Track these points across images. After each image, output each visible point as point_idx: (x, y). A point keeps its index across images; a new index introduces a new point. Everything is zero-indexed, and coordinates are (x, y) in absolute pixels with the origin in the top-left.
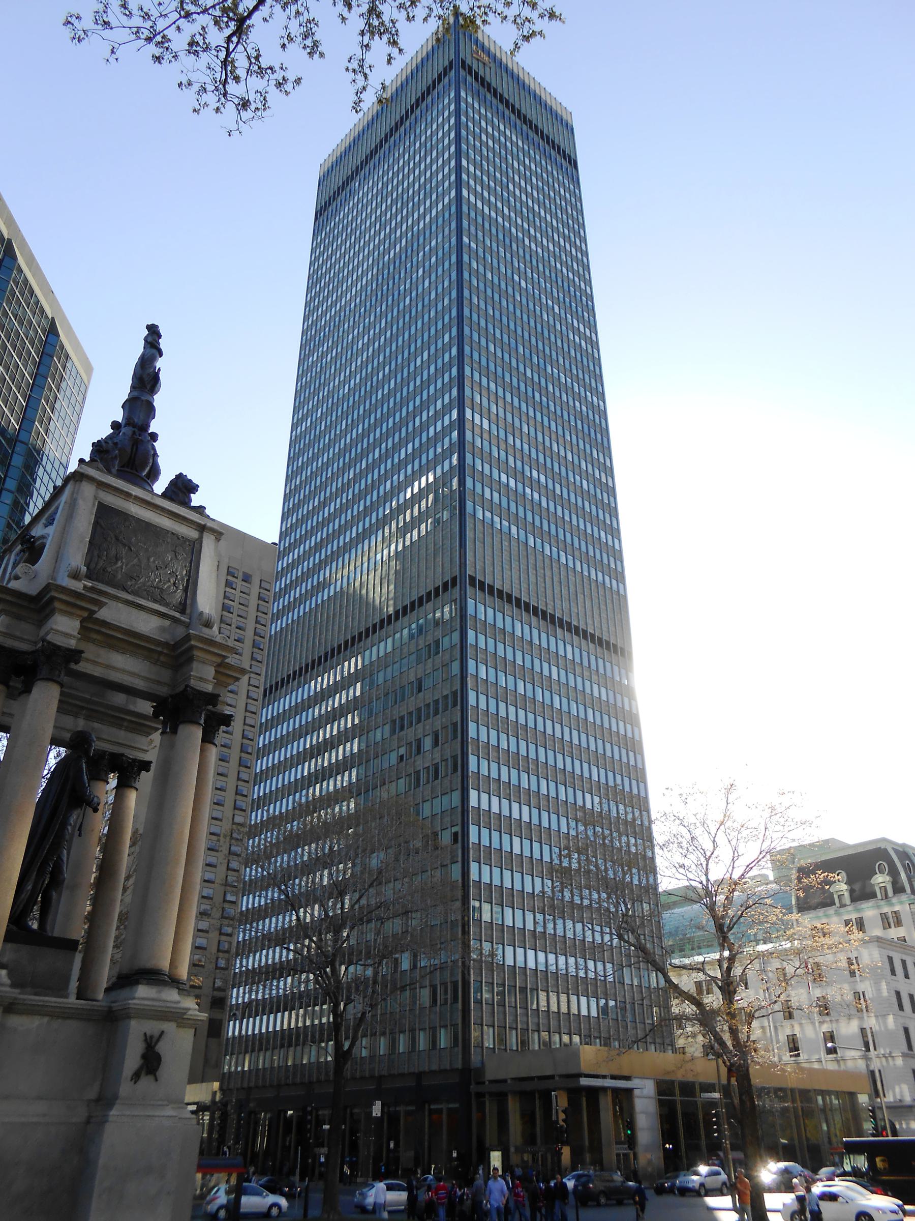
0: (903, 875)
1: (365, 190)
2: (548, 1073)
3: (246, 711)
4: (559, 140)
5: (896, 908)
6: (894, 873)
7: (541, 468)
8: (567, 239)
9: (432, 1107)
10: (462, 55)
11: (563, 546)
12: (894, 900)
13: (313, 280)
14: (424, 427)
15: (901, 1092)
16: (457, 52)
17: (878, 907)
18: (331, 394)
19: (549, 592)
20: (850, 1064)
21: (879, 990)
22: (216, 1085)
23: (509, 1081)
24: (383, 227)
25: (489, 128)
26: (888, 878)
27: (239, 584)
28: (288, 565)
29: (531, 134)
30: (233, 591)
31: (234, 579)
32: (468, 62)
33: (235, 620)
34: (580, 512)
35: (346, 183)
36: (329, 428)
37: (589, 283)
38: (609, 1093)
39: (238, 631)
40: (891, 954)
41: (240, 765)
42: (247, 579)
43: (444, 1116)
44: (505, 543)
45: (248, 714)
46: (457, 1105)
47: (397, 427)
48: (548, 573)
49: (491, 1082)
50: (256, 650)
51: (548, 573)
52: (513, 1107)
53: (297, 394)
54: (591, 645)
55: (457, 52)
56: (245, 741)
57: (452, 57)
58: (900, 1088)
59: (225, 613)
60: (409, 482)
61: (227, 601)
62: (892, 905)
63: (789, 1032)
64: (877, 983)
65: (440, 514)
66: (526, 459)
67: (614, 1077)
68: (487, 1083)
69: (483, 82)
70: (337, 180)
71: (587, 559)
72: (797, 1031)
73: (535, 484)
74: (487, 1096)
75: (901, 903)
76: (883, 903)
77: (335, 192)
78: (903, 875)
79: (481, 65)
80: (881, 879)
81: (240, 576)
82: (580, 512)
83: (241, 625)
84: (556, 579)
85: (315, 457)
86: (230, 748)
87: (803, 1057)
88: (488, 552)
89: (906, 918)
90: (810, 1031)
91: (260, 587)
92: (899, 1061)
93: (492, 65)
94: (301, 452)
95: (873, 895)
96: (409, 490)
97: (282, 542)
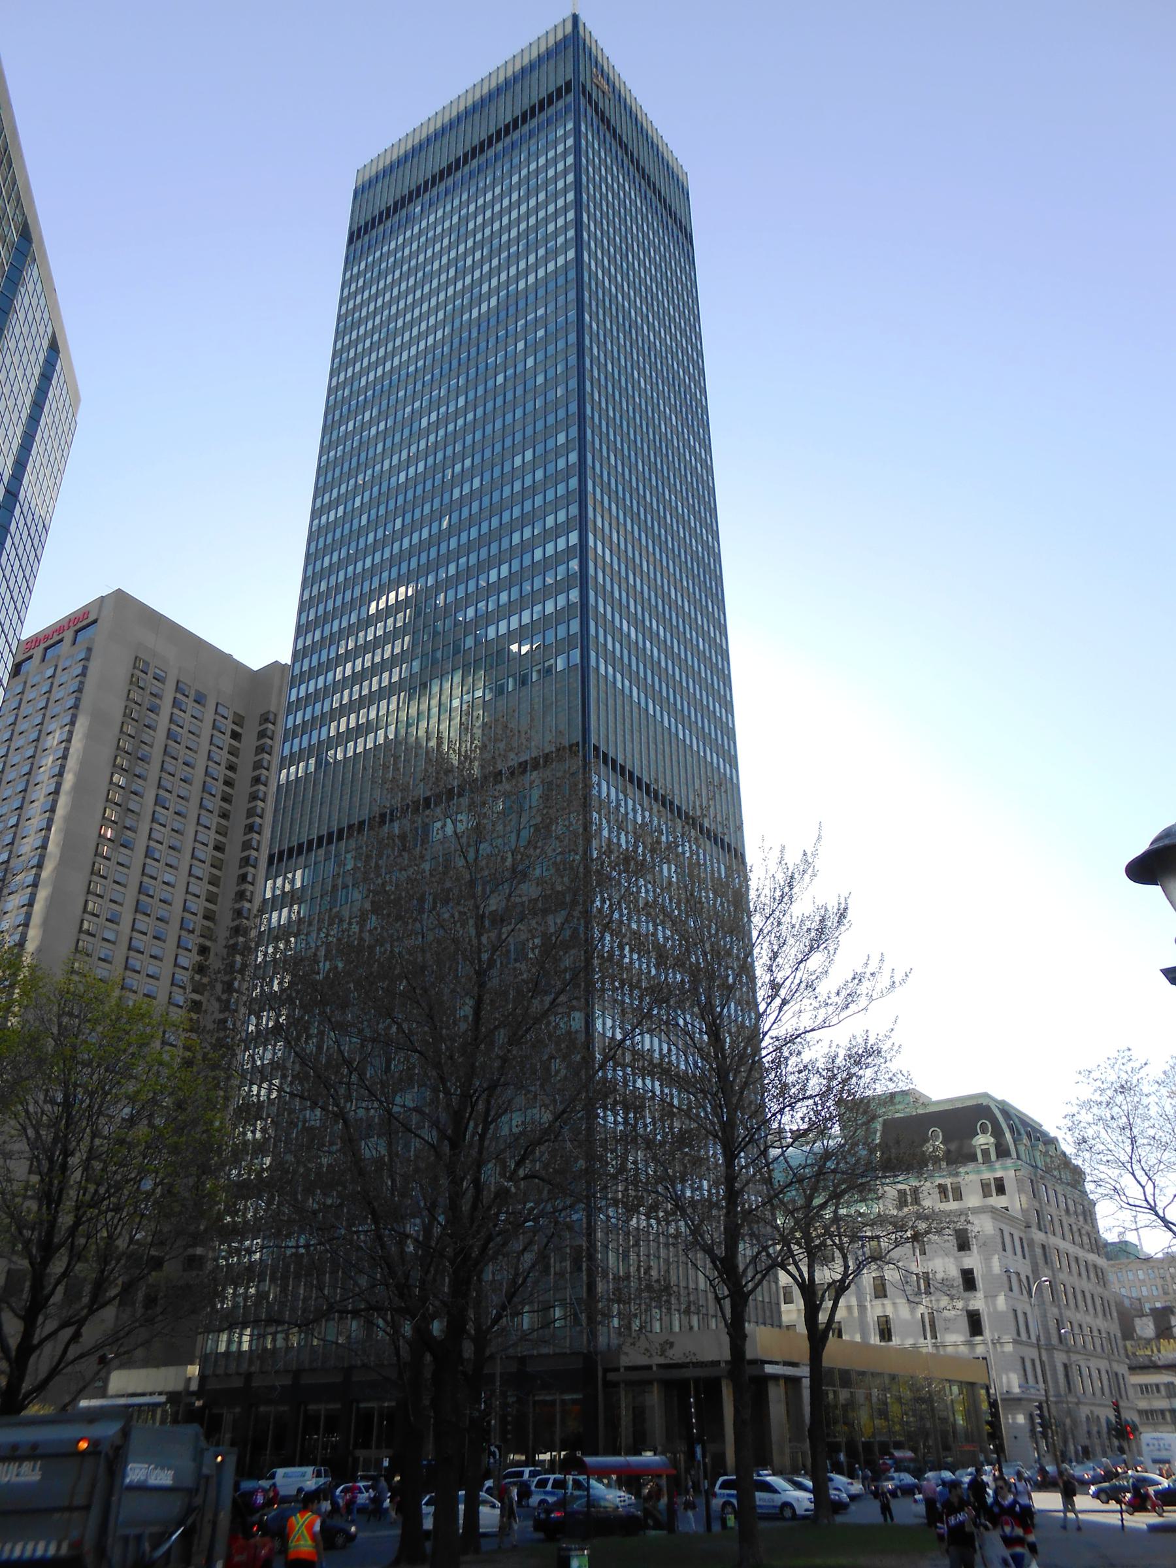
0: (1008, 1135)
1: (434, 220)
2: (716, 1358)
3: (190, 875)
4: (676, 205)
5: (998, 1175)
6: (998, 1133)
7: (660, 618)
8: (683, 332)
9: (537, 1398)
10: (582, 79)
11: (684, 720)
12: (998, 1165)
13: (346, 324)
14: (527, 547)
15: (1009, 1382)
16: (576, 71)
17: (979, 1172)
18: (377, 480)
19: (668, 772)
20: (950, 1350)
21: (989, 1267)
22: (194, 1370)
23: (655, 1368)
24: (461, 274)
25: (609, 180)
26: (992, 1140)
27: (190, 705)
28: (308, 695)
29: (650, 193)
30: (182, 714)
31: (184, 698)
32: (588, 88)
33: (182, 753)
34: (694, 675)
35: (400, 204)
36: (374, 524)
37: (704, 391)
38: (782, 1382)
39: (186, 768)
40: (1004, 1227)
41: (178, 947)
42: (199, 700)
43: (558, 1408)
44: (627, 708)
45: (192, 880)
46: (338, 1406)
47: (484, 540)
48: (667, 749)
49: (628, 1368)
50: (206, 795)
51: (667, 749)
52: (654, 1398)
53: (321, 471)
54: (708, 842)
55: (576, 71)
56: (187, 915)
57: (570, 76)
58: (1008, 1378)
59: (171, 742)
60: (383, 590)
61: (173, 727)
62: (994, 1170)
63: (879, 1312)
64: (987, 1260)
65: (552, 661)
66: (646, 605)
67: (786, 1364)
68: (622, 1370)
69: (603, 118)
70: (385, 197)
71: (703, 737)
72: (889, 1311)
73: (653, 637)
74: (622, 1385)
75: (1005, 1169)
76: (983, 1167)
77: (385, 209)
78: (1008, 1135)
79: (600, 94)
80: (983, 1140)
81: (192, 697)
82: (694, 675)
83: (191, 760)
84: (674, 758)
85: (350, 560)
86: (167, 923)
87: (896, 1341)
88: (611, 717)
89: (1009, 1185)
90: (898, 1310)
91: (216, 713)
92: (1009, 1348)
93: (611, 96)
94: (328, 550)
95: (973, 1158)
96: (374, 605)
97: (298, 665)
